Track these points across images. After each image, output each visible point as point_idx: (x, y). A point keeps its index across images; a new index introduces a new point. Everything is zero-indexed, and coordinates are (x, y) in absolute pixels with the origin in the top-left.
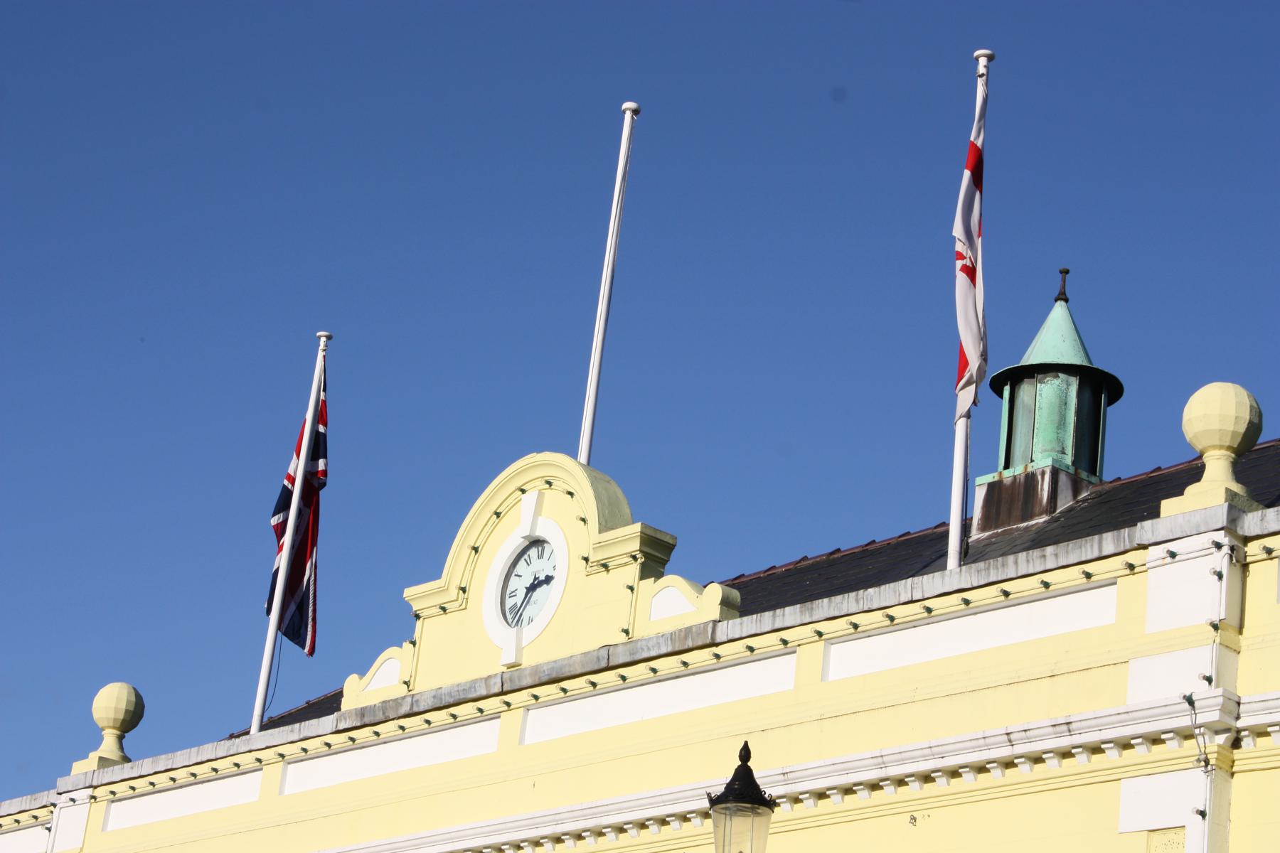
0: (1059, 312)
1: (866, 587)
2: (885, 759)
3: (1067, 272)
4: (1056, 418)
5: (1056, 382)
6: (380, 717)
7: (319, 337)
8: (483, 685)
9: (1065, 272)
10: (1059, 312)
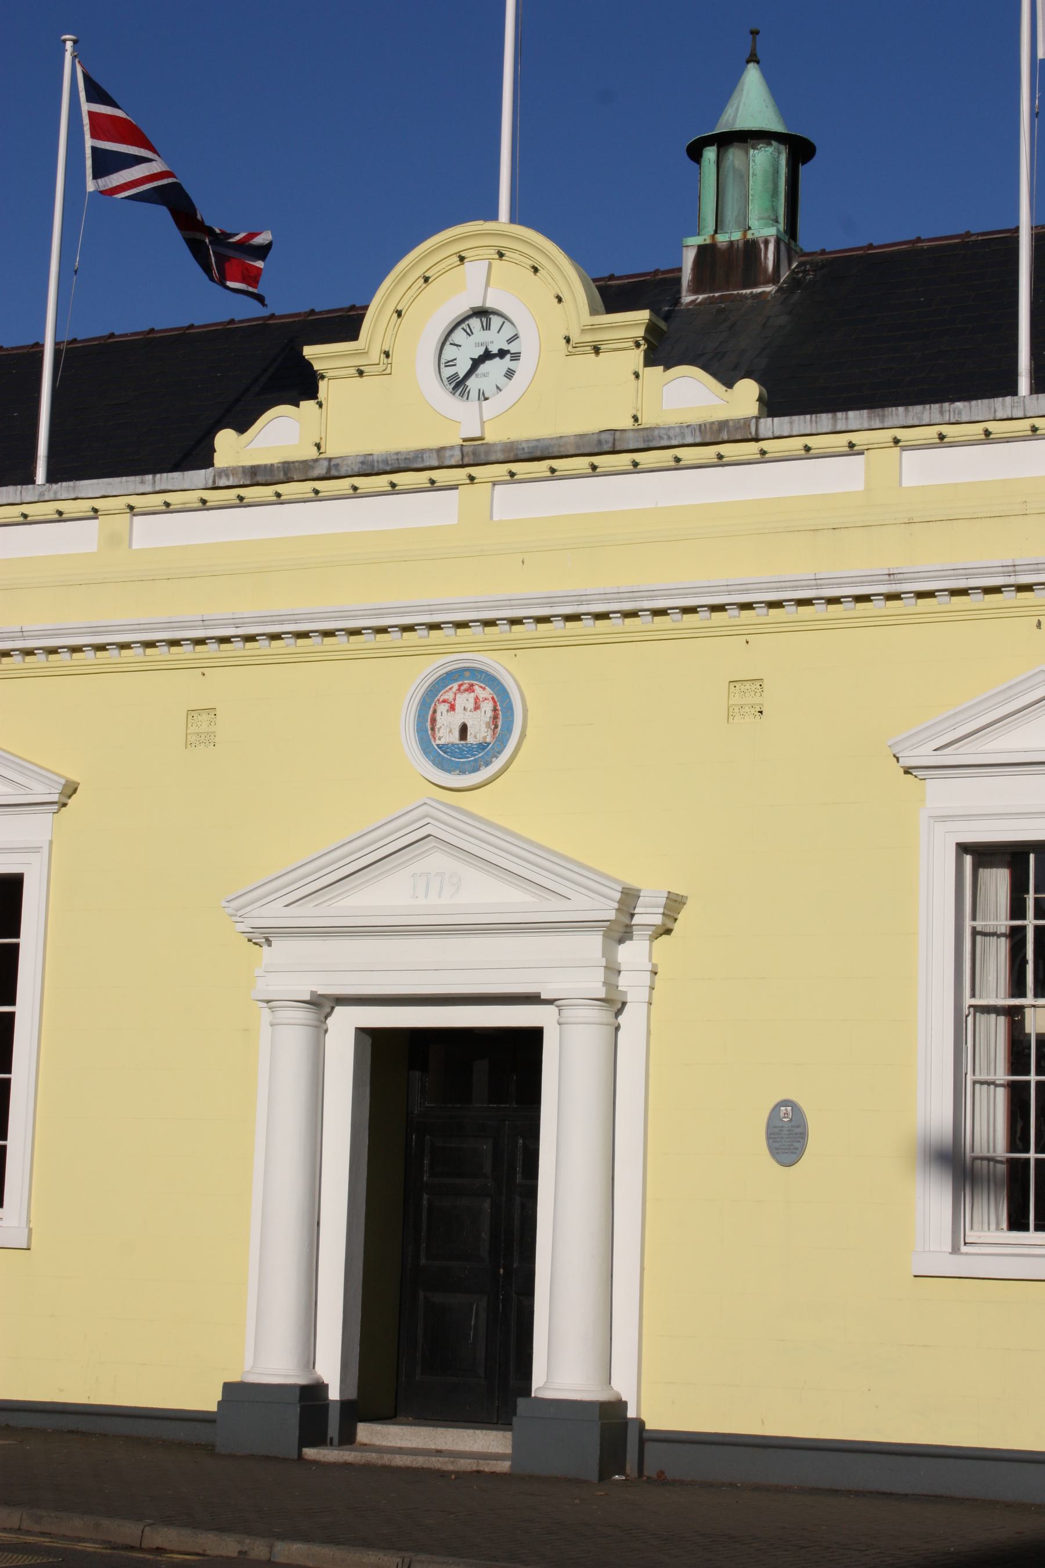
0: (752, 76)
1: (952, 401)
2: (1017, 568)
3: (757, 33)
4: (770, 185)
5: (770, 149)
6: (282, 477)
7: (64, 41)
8: (435, 455)
9: (755, 33)
10: (752, 76)
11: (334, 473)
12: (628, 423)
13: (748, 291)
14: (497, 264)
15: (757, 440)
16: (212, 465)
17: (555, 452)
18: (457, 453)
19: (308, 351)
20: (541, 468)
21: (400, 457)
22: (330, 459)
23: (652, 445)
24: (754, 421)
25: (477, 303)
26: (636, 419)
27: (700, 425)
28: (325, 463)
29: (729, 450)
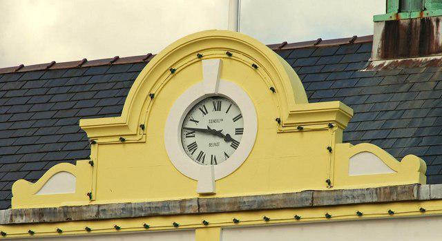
11: (102, 216)
12: (323, 187)
13: (424, 58)
14: (226, 61)
15: (418, 201)
16: (10, 206)
17: (268, 205)
18: (195, 204)
19: (83, 123)
20: (258, 218)
21: (151, 205)
22: (99, 206)
23: (340, 203)
24: (416, 187)
25: (211, 90)
26: (328, 182)
27: (376, 189)
28: (96, 209)
29: (399, 209)
